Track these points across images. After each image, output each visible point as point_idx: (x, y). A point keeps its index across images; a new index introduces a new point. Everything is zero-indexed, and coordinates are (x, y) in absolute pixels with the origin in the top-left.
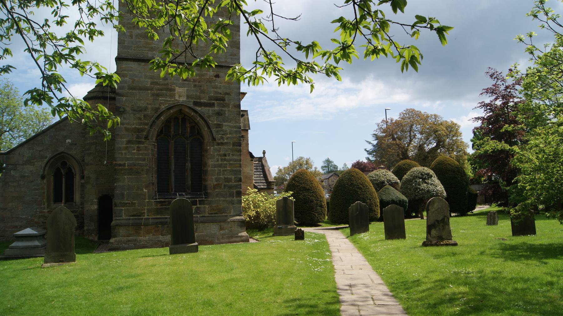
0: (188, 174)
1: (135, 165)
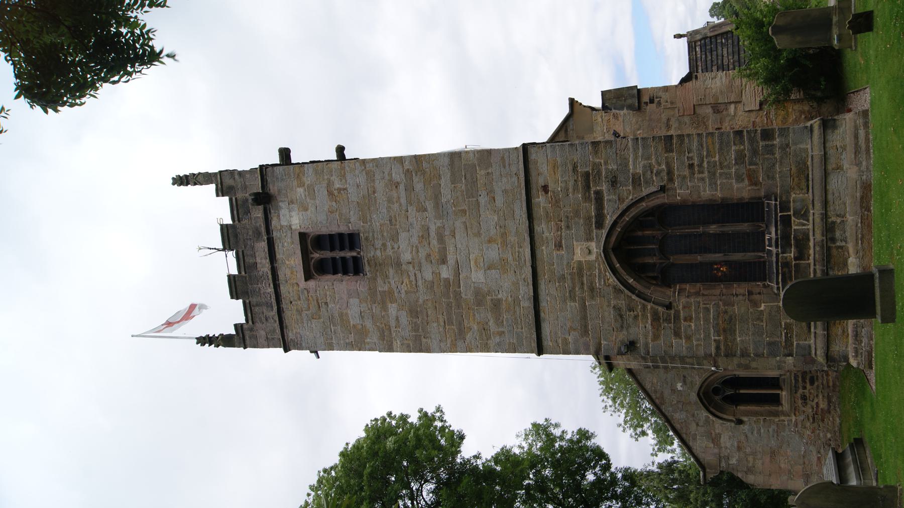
0: (730, 228)
1: (718, 324)
